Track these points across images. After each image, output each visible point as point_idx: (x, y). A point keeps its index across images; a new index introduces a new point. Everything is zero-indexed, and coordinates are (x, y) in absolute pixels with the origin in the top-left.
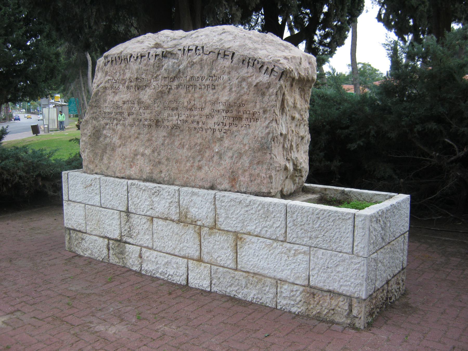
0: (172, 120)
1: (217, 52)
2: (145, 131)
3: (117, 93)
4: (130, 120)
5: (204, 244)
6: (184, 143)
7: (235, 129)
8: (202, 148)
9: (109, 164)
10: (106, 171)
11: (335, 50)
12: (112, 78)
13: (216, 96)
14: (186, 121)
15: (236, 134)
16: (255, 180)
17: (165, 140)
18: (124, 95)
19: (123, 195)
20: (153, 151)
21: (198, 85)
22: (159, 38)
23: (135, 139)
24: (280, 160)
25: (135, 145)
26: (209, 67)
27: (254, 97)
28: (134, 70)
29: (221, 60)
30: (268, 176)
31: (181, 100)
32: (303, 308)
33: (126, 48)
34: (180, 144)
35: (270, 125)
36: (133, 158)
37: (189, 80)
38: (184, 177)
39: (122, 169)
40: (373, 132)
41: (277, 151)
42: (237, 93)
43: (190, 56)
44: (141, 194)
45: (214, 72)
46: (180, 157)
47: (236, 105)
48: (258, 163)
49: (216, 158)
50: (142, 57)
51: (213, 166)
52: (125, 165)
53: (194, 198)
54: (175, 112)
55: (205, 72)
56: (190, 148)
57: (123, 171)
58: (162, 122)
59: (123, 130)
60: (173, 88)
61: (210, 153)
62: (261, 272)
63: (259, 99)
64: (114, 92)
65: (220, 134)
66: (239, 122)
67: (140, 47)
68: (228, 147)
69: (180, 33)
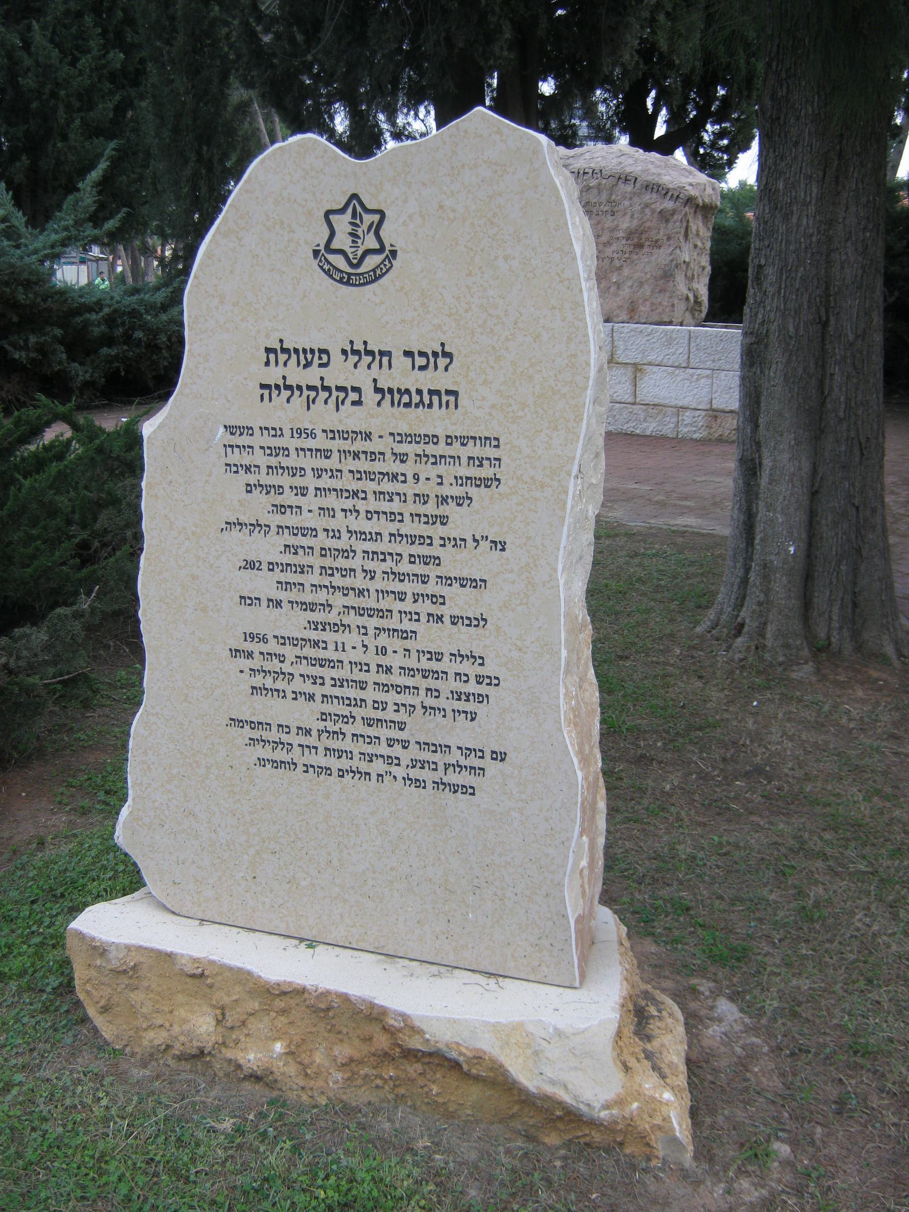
11: (737, 158)
24: (682, 288)
29: (621, 185)
32: (705, 433)
41: (680, 278)
45: (613, 197)
48: (660, 291)
49: (613, 289)
55: (604, 196)
62: (662, 402)
63: (663, 226)
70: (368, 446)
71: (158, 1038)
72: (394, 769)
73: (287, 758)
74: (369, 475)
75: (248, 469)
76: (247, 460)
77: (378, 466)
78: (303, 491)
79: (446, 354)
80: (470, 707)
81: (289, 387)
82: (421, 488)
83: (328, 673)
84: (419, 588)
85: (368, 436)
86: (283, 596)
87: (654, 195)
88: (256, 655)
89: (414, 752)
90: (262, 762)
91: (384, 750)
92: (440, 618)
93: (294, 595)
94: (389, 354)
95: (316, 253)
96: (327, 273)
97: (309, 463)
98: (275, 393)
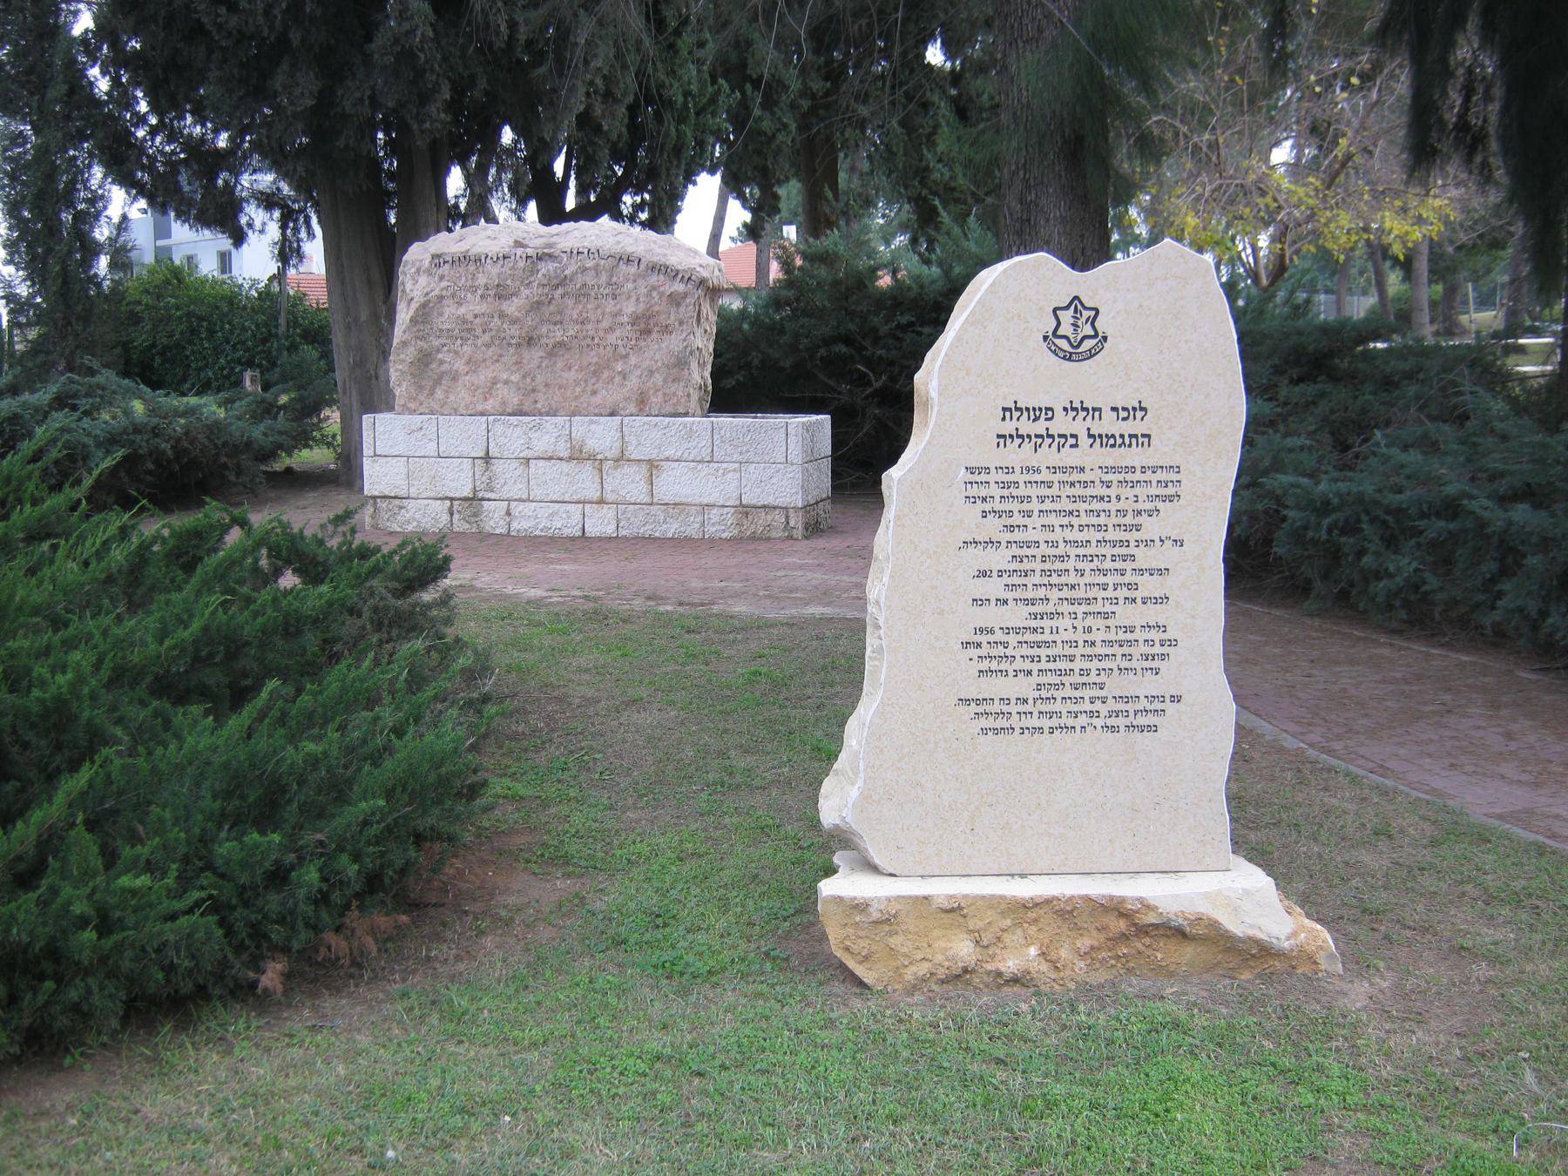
5: (608, 480)
18: (473, 306)
29: (623, 267)
32: (736, 532)
40: (756, 362)
53: (593, 427)
55: (604, 278)
56: (581, 369)
70: (1082, 477)
71: (923, 969)
72: (1095, 721)
73: (1005, 724)
74: (1083, 499)
75: (984, 499)
76: (983, 492)
77: (1090, 491)
78: (1029, 514)
79: (1142, 409)
80: (1154, 664)
81: (1019, 436)
82: (1122, 505)
83: (1043, 652)
84: (1119, 579)
85: (1082, 470)
86: (1010, 595)
87: (662, 277)
88: (984, 644)
89: (1112, 705)
90: (985, 731)
91: (1087, 707)
92: (1134, 600)
93: (1018, 594)
94: (1100, 410)
95: (1045, 338)
96: (1054, 352)
97: (1034, 492)
98: (1009, 441)
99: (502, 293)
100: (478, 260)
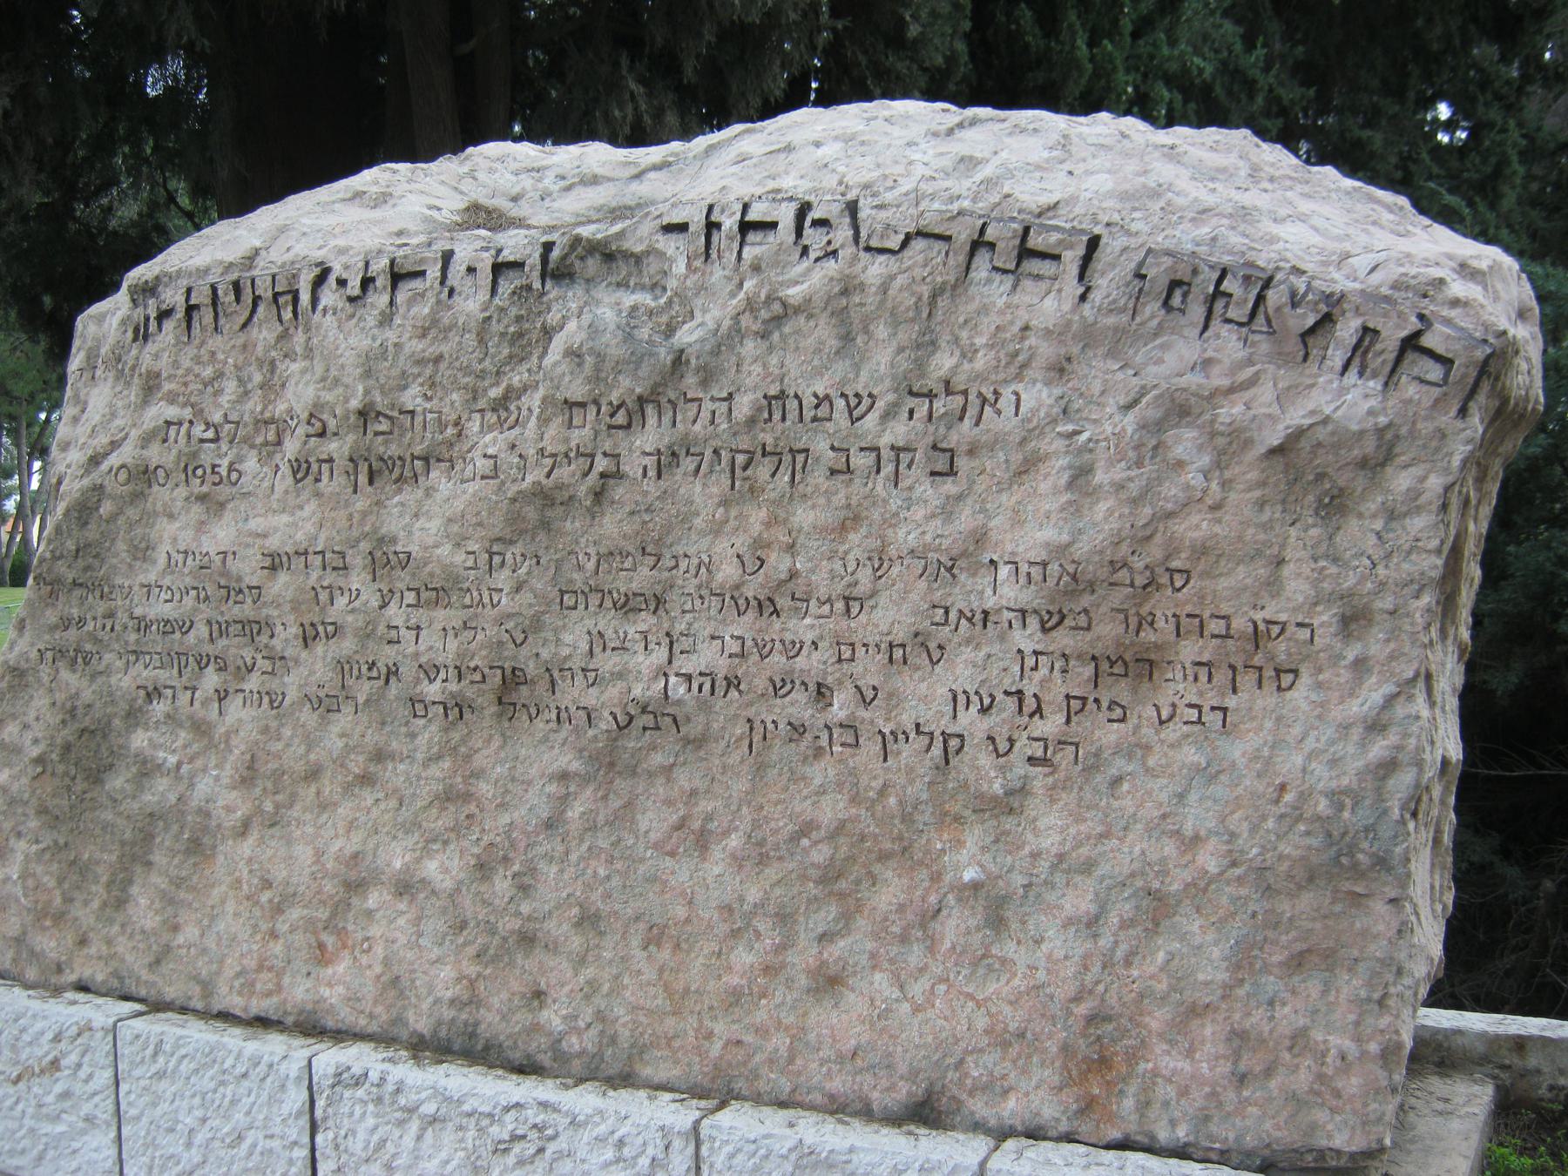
0: (620, 676)
1: (963, 234)
2: (422, 740)
3: (222, 505)
4: (314, 668)
6: (709, 818)
7: (1110, 735)
8: (851, 859)
9: (166, 937)
10: (145, 975)
12: (187, 413)
13: (966, 519)
14: (732, 683)
15: (1120, 765)
16: (1269, 1072)
17: (564, 800)
18: (271, 517)
19: (276, 1144)
20: (483, 869)
21: (821, 446)
22: (481, 176)
23: (348, 788)
25: (351, 826)
26: (907, 334)
27: (1266, 527)
28: (349, 358)
29: (990, 289)
30: (1373, 1047)
31: (695, 546)
33: (283, 230)
34: (680, 826)
35: (1400, 710)
36: (340, 907)
37: (751, 421)
38: (710, 1035)
39: (260, 968)
42: (1135, 502)
43: (756, 268)
44: (408, 1141)
45: (943, 362)
46: (681, 912)
47: (1124, 575)
48: (1297, 963)
50: (397, 277)
51: (937, 969)
52: (277, 948)
54: (645, 621)
55: (882, 359)
56: (759, 855)
57: (264, 981)
58: (543, 685)
59: (265, 730)
60: (632, 467)
61: (911, 889)
63: (1300, 540)
64: (202, 498)
65: (1002, 769)
66: (1135, 691)
67: (376, 222)
68: (1061, 857)
69: (597, 155)
87: (1227, 343)
99: (381, 450)
100: (285, 296)
